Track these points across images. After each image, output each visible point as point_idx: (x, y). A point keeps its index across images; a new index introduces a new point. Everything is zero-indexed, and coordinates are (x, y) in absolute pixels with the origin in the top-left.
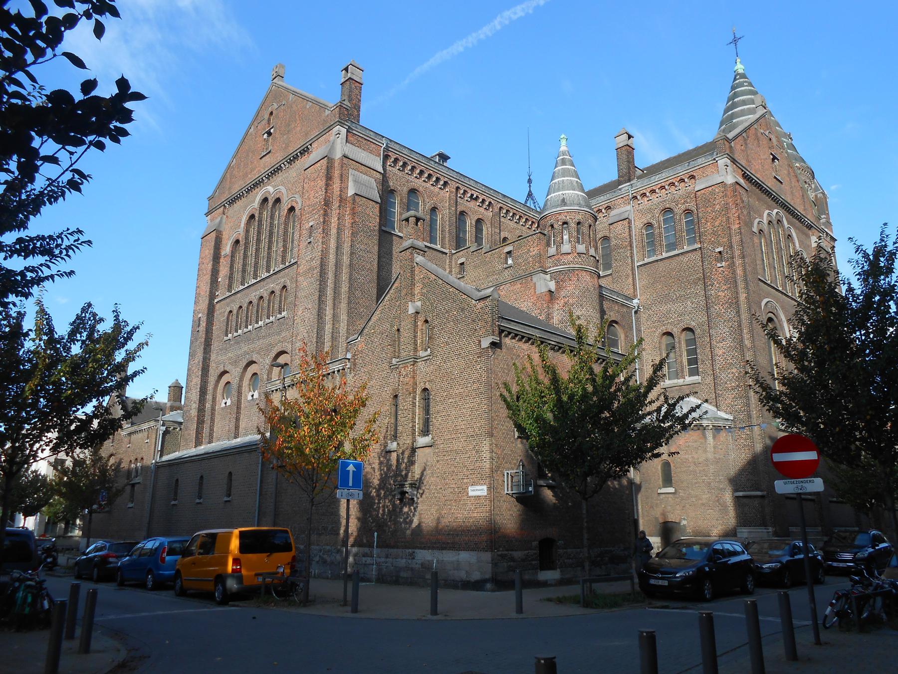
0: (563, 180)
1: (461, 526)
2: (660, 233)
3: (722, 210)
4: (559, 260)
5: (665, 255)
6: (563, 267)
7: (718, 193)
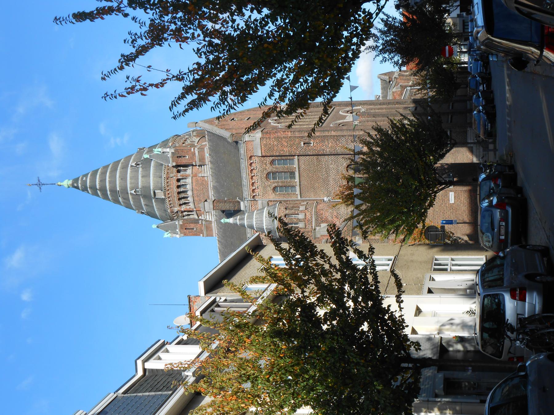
0: (256, 218)
1: (467, 208)
2: (282, 182)
3: (278, 140)
4: (309, 220)
5: (297, 180)
6: (313, 218)
7: (266, 142)
